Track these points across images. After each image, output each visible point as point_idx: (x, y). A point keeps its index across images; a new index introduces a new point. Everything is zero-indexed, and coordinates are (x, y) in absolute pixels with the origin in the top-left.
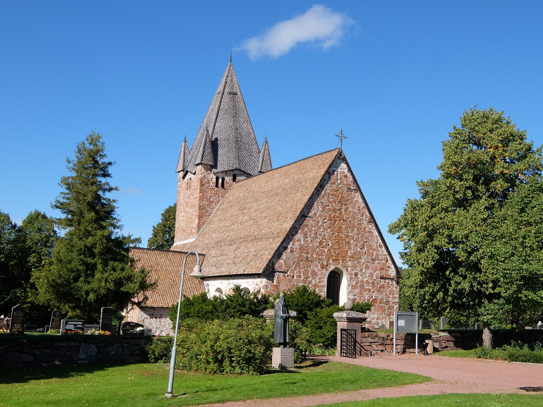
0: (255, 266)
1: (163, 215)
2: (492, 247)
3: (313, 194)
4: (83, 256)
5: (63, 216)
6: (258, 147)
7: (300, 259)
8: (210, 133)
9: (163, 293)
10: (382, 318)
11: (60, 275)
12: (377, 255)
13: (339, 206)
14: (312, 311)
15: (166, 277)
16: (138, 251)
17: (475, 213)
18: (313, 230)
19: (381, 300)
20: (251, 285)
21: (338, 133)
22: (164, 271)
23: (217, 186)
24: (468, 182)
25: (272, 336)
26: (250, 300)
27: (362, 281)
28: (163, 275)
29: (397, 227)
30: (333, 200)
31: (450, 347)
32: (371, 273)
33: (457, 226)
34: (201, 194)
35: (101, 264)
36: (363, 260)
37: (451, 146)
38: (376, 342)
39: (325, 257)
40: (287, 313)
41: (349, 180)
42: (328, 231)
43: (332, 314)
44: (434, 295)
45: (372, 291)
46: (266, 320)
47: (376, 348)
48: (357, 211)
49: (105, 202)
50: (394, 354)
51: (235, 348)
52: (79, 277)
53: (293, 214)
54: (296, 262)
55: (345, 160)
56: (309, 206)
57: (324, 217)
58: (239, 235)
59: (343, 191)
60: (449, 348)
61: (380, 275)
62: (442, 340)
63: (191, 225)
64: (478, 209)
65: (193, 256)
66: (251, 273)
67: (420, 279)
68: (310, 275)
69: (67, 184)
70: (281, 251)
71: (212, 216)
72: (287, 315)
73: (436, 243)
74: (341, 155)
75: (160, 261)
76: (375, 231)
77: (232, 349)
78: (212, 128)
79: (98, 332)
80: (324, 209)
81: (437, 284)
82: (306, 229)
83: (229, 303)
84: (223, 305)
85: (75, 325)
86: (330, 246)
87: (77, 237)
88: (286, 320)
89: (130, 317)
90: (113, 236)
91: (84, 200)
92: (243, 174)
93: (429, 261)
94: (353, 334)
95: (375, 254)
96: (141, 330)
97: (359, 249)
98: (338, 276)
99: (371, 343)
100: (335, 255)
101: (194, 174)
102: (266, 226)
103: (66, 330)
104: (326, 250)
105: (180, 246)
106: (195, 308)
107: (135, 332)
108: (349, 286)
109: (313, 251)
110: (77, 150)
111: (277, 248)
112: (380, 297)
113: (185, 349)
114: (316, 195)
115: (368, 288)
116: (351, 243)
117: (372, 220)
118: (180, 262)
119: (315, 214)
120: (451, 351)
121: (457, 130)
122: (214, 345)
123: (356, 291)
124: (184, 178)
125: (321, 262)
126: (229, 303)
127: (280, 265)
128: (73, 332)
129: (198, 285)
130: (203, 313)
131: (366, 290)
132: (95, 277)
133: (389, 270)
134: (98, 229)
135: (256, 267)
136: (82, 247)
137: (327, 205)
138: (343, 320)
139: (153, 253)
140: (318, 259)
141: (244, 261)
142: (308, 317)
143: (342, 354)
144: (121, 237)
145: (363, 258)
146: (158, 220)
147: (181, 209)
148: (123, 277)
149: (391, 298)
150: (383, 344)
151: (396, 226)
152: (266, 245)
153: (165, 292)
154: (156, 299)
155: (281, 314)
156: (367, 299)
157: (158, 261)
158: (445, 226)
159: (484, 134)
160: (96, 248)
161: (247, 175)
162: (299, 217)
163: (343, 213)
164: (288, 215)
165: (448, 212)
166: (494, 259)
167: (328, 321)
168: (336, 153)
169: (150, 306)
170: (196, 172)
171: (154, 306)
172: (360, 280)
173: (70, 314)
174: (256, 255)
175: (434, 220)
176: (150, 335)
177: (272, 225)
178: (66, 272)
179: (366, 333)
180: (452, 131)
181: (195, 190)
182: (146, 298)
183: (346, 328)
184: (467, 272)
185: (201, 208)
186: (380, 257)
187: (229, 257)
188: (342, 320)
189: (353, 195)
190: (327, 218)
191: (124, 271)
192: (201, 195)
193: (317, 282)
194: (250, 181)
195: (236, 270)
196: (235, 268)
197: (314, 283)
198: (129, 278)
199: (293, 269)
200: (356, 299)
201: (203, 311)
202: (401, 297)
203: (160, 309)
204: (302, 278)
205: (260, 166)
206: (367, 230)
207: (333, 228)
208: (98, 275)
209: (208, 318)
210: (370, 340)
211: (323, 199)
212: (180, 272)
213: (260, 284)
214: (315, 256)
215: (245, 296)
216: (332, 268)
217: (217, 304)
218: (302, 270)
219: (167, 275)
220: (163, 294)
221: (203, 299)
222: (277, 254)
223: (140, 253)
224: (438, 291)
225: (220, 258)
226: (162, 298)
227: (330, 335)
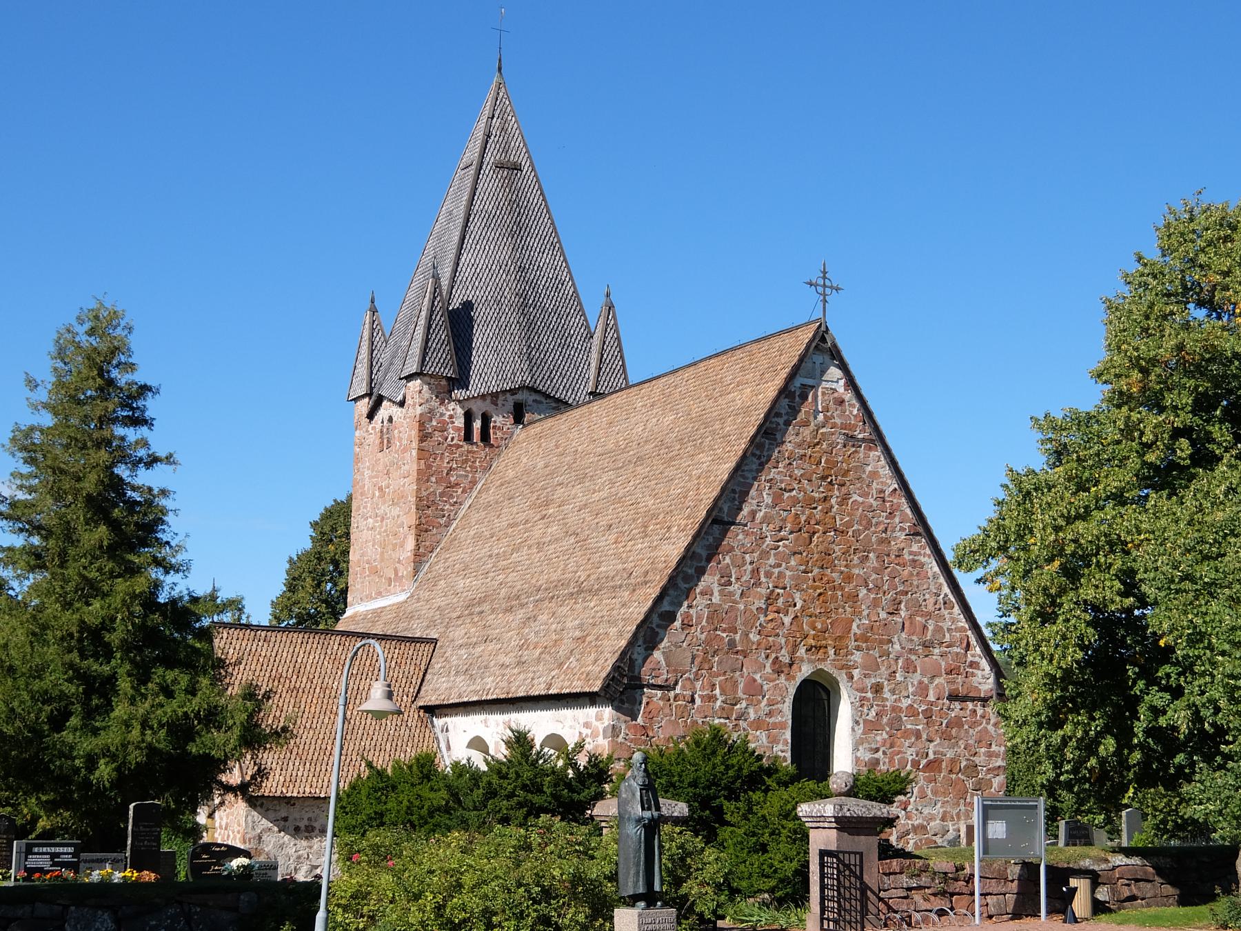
0: (579, 670)
1: (314, 525)
2: (1195, 611)
3: (744, 457)
4: (75, 657)
5: (18, 541)
6: (587, 321)
7: (710, 649)
8: (445, 283)
9: (316, 754)
10: (958, 815)
11: (12, 710)
12: (939, 630)
13: (821, 489)
14: (737, 799)
15: (324, 707)
16: (241, 635)
17: (1201, 503)
18: (748, 561)
19: (953, 761)
20: (571, 727)
21: (815, 276)
22: (318, 690)
23: (468, 437)
24: (1178, 416)
25: (613, 877)
26: (553, 772)
27: (894, 709)
28: (315, 702)
29: (978, 551)
30: (802, 471)
31: (1142, 899)
32: (920, 683)
33: (1148, 545)
34: (423, 461)
35: (129, 675)
36: (897, 647)
37: (1130, 312)
38: (925, 888)
39: (783, 641)
40: (653, 809)
41: (851, 412)
42: (793, 563)
43: (795, 808)
44: (1089, 746)
45: (924, 736)
46: (601, 828)
47: (923, 905)
48: (875, 504)
49: (136, 496)
50: (977, 922)
51: (504, 911)
52: (66, 715)
53: (688, 517)
54: (699, 656)
55: (835, 355)
56: (734, 491)
57: (778, 524)
58: (534, 581)
59: (832, 445)
60: (1139, 901)
61: (949, 689)
62: (1118, 879)
63: (395, 555)
64: (1208, 492)
65: (403, 647)
66: (567, 691)
67: (1045, 699)
68: (740, 694)
69: (24, 448)
70: (654, 626)
71: (456, 528)
72: (656, 814)
73: (1088, 593)
74: (823, 339)
75: (305, 661)
76: (929, 561)
77: (496, 914)
78: (450, 269)
79: (123, 874)
80: (776, 502)
81: (1097, 715)
82: (728, 560)
83: (495, 780)
84: (479, 789)
85: (54, 856)
86: (798, 606)
87: (57, 601)
88: (651, 828)
89: (221, 827)
90: (164, 595)
91: (77, 491)
92: (544, 401)
93: (1068, 649)
94: (855, 865)
95: (931, 628)
96: (243, 866)
97: (883, 615)
98: (825, 697)
99: (909, 889)
100: (813, 632)
101: (402, 404)
102: (611, 552)
103: (27, 869)
104: (787, 620)
105: (365, 616)
106: (400, 799)
107: (226, 873)
108: (857, 723)
109: (749, 624)
110: (53, 349)
111: (641, 617)
112: (950, 754)
113: (362, 916)
114: (755, 460)
115: (914, 727)
116: (861, 595)
117: (920, 529)
118: (362, 663)
119: (753, 514)
120: (1145, 910)
121: (1145, 265)
122: (444, 906)
123: (879, 738)
124: (371, 416)
125: (774, 656)
126: (495, 780)
127: (651, 666)
128: (48, 876)
129: (418, 731)
130: (424, 812)
131: (907, 734)
132: (112, 715)
133: (973, 675)
134: (119, 576)
135: (582, 674)
136: (74, 629)
137: (788, 488)
138: (826, 825)
139: (284, 638)
140: (763, 646)
141: (547, 657)
142: (728, 817)
143: (825, 922)
144: (187, 598)
145: (895, 639)
146: (303, 541)
147: (365, 507)
148: (192, 711)
149: (983, 758)
150: (943, 893)
151: (977, 547)
152: (613, 609)
153: (322, 754)
154: (294, 774)
155: (637, 810)
156: (910, 759)
157: (299, 661)
158: (1115, 544)
159: (1226, 274)
160: (115, 630)
161: (554, 405)
162: (706, 526)
163: (834, 510)
164: (673, 519)
165: (1123, 504)
166: (1201, 646)
167: (784, 827)
168: (810, 335)
169: (278, 794)
170: (404, 398)
171: (289, 795)
172: (888, 704)
173: (43, 824)
174: (582, 639)
175: (1080, 526)
176: (272, 879)
177: (628, 549)
178: (29, 703)
179: (895, 862)
180: (1134, 267)
181: (405, 451)
182: (261, 773)
183: (833, 847)
184: (1182, 679)
185: (423, 504)
186: (947, 635)
187: (505, 645)
188: (821, 825)
189: (861, 455)
190: (789, 525)
191: (194, 695)
192: (423, 466)
193: (761, 713)
194: (563, 422)
195: (527, 682)
196: (522, 676)
197: (752, 716)
198: (213, 717)
199: (692, 677)
200: (877, 761)
201: (423, 807)
202: (1019, 753)
203: (307, 803)
204: (719, 703)
205: (591, 378)
206: (907, 557)
207: (804, 554)
208: (121, 710)
209: (437, 825)
210: (905, 880)
211: (773, 470)
212: (364, 694)
213: (595, 723)
214: (754, 637)
215: (541, 762)
216: (805, 671)
217: (460, 786)
218: (717, 681)
219: (325, 702)
220: (315, 759)
221: (422, 772)
222: (642, 634)
223: (246, 641)
224: (1100, 735)
225: (479, 649)
226: (312, 770)
227: (790, 867)
